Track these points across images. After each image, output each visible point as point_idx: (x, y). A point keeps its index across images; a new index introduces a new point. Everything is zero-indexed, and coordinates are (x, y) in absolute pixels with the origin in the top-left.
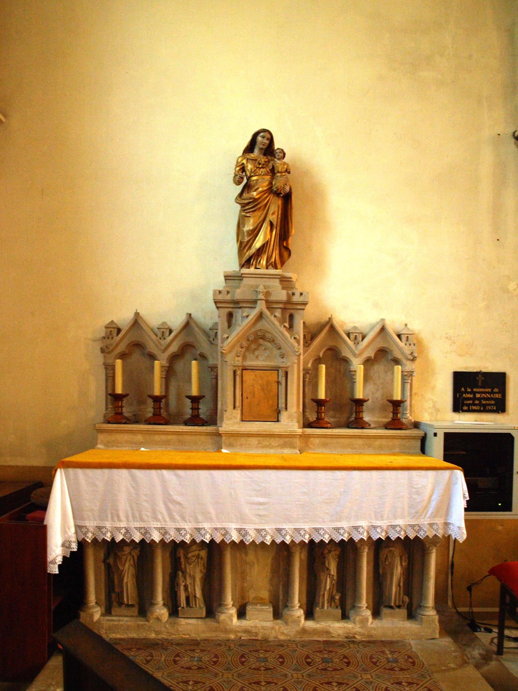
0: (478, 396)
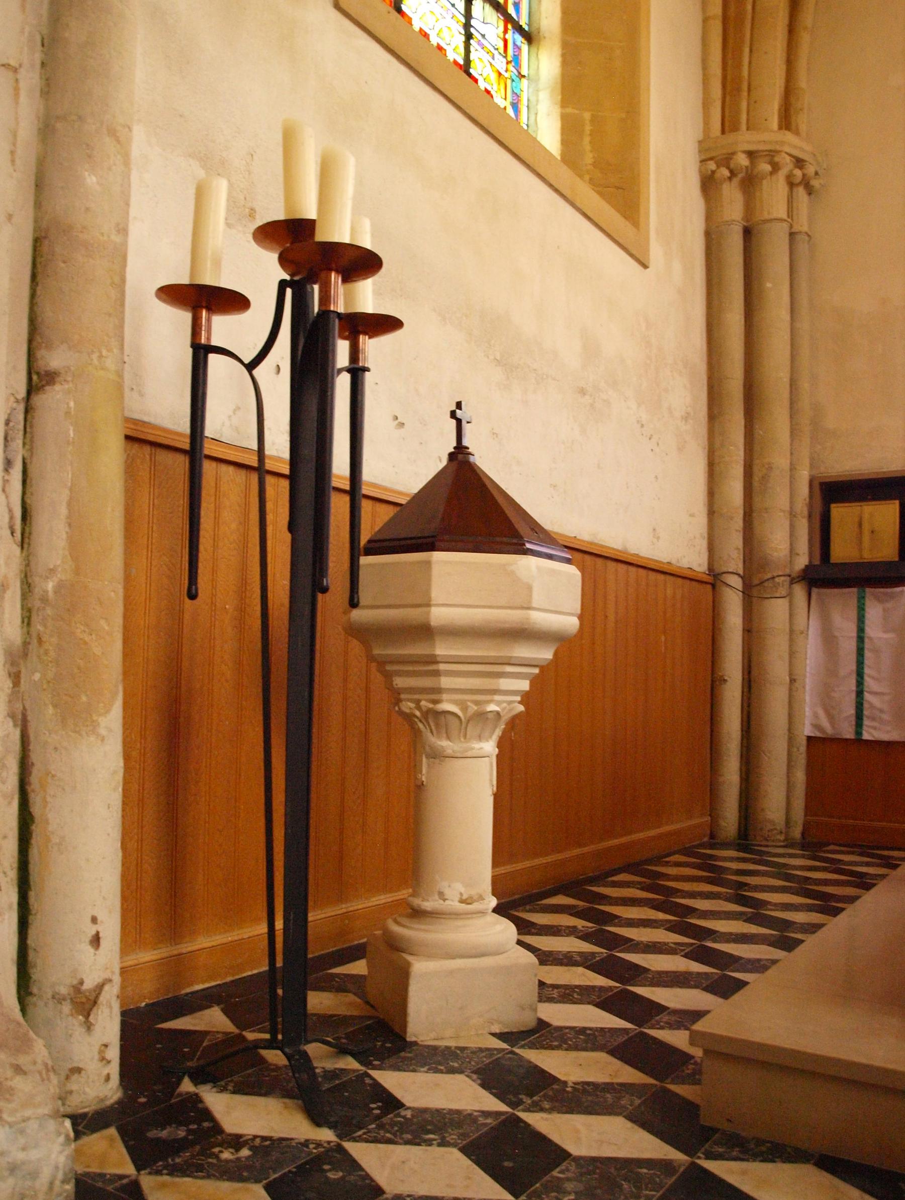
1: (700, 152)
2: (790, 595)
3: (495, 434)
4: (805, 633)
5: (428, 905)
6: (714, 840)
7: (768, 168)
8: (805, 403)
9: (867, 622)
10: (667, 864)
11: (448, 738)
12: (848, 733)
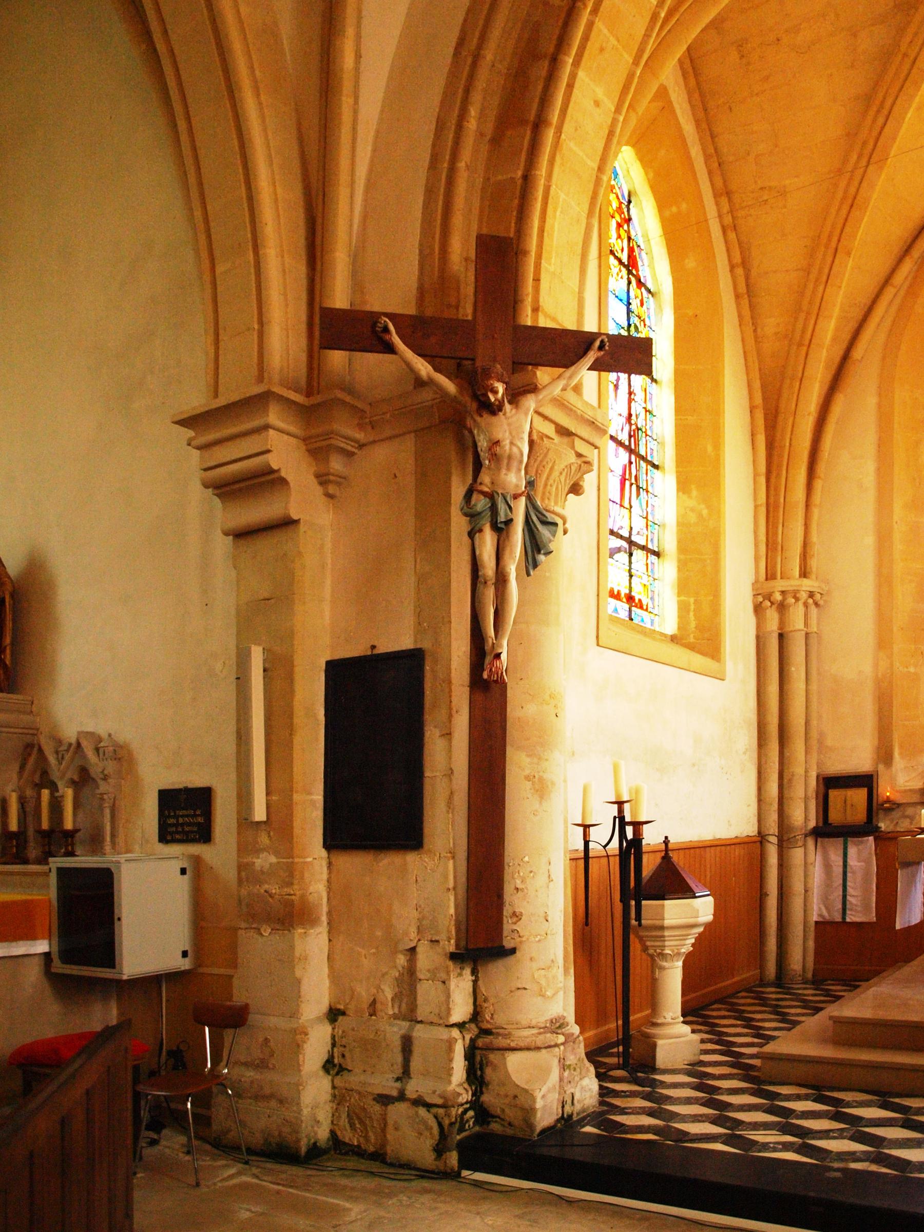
0: (181, 820)
1: (753, 589)
2: (805, 846)
3: (657, 805)
4: (813, 864)
5: (659, 1021)
6: (762, 982)
7: (793, 600)
8: (814, 734)
9: (848, 856)
10: (738, 998)
11: (666, 961)
12: (838, 918)
